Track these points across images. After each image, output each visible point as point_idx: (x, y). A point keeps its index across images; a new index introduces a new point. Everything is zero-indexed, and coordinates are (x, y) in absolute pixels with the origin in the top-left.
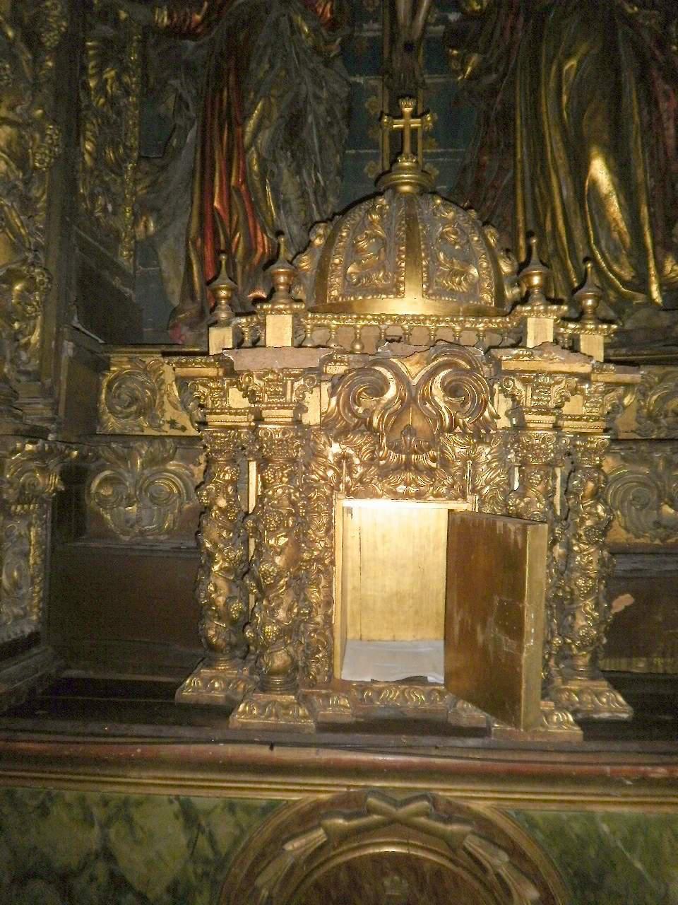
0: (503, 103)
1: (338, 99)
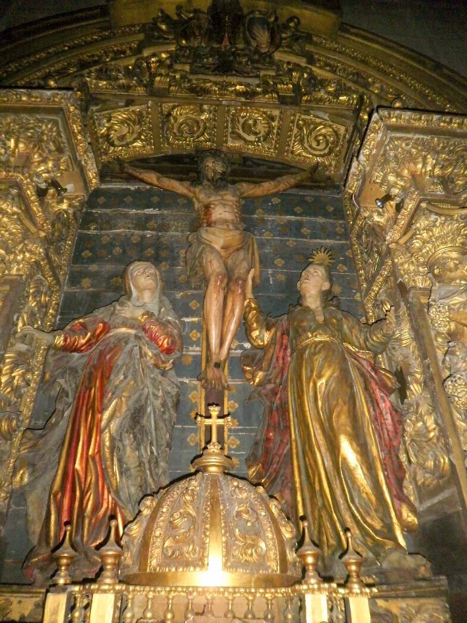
0: (280, 399)
1: (169, 395)
